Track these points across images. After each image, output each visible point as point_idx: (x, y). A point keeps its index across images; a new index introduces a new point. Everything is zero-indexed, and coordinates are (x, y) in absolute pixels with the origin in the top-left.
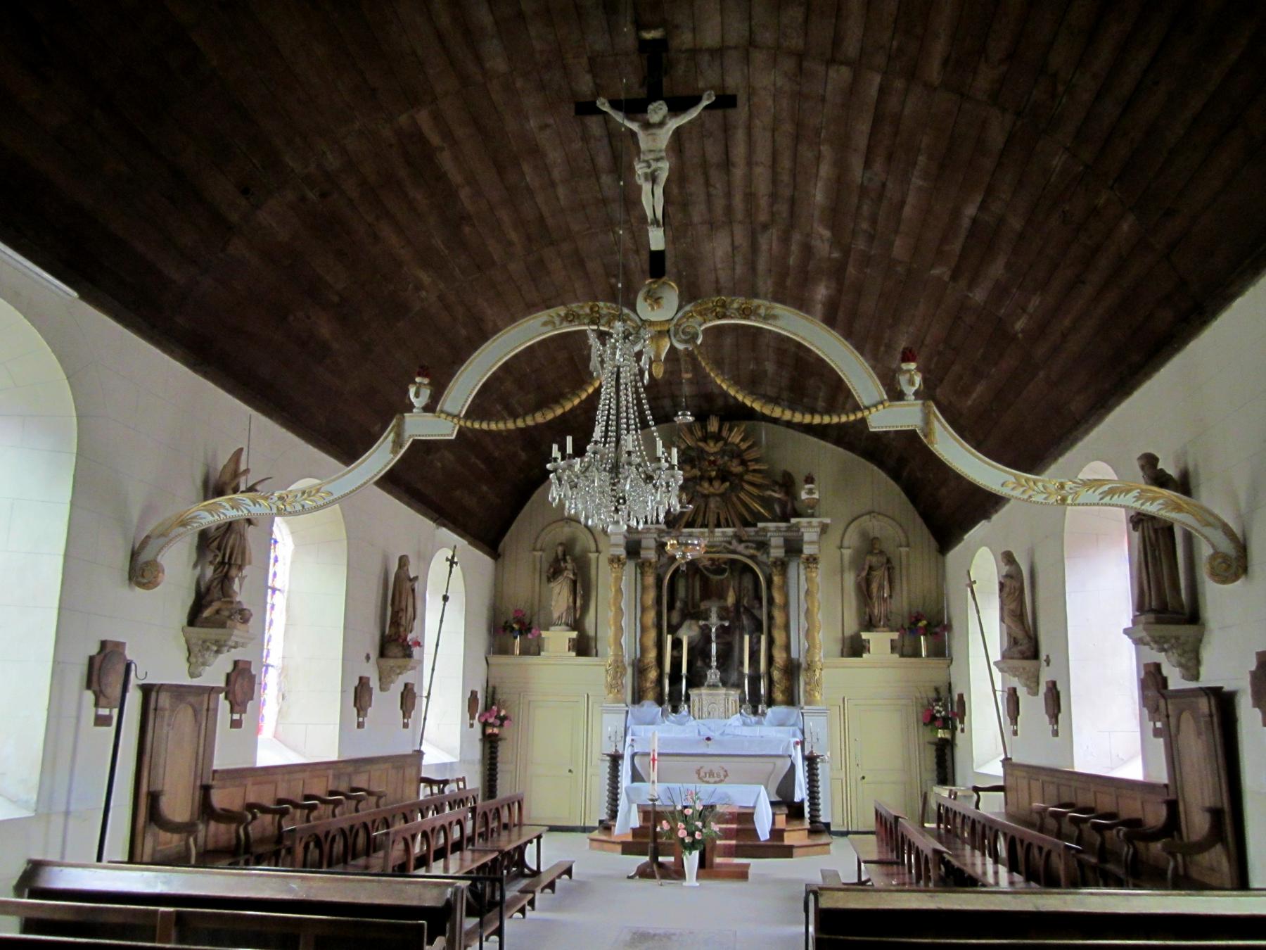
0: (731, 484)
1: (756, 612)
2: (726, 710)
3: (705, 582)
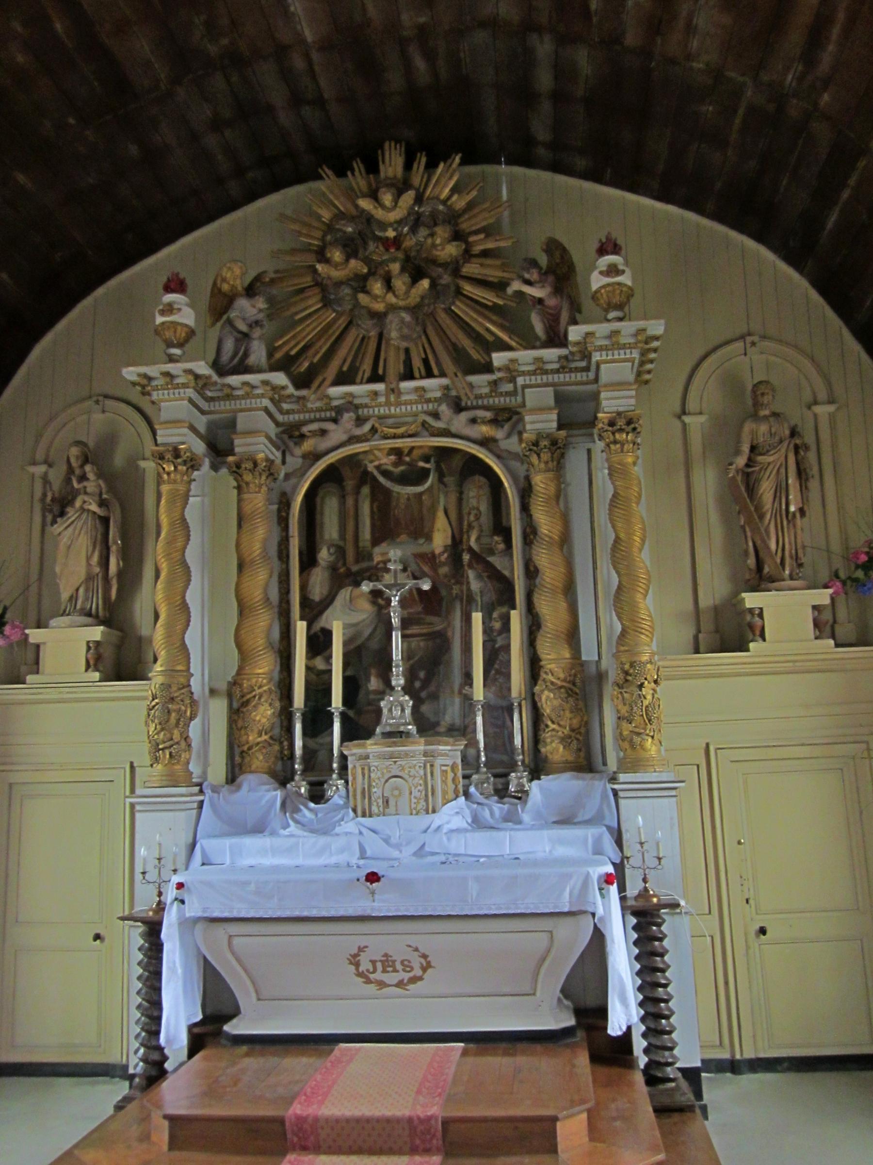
0: (433, 285)
1: (496, 561)
2: (429, 793)
3: (383, 499)
